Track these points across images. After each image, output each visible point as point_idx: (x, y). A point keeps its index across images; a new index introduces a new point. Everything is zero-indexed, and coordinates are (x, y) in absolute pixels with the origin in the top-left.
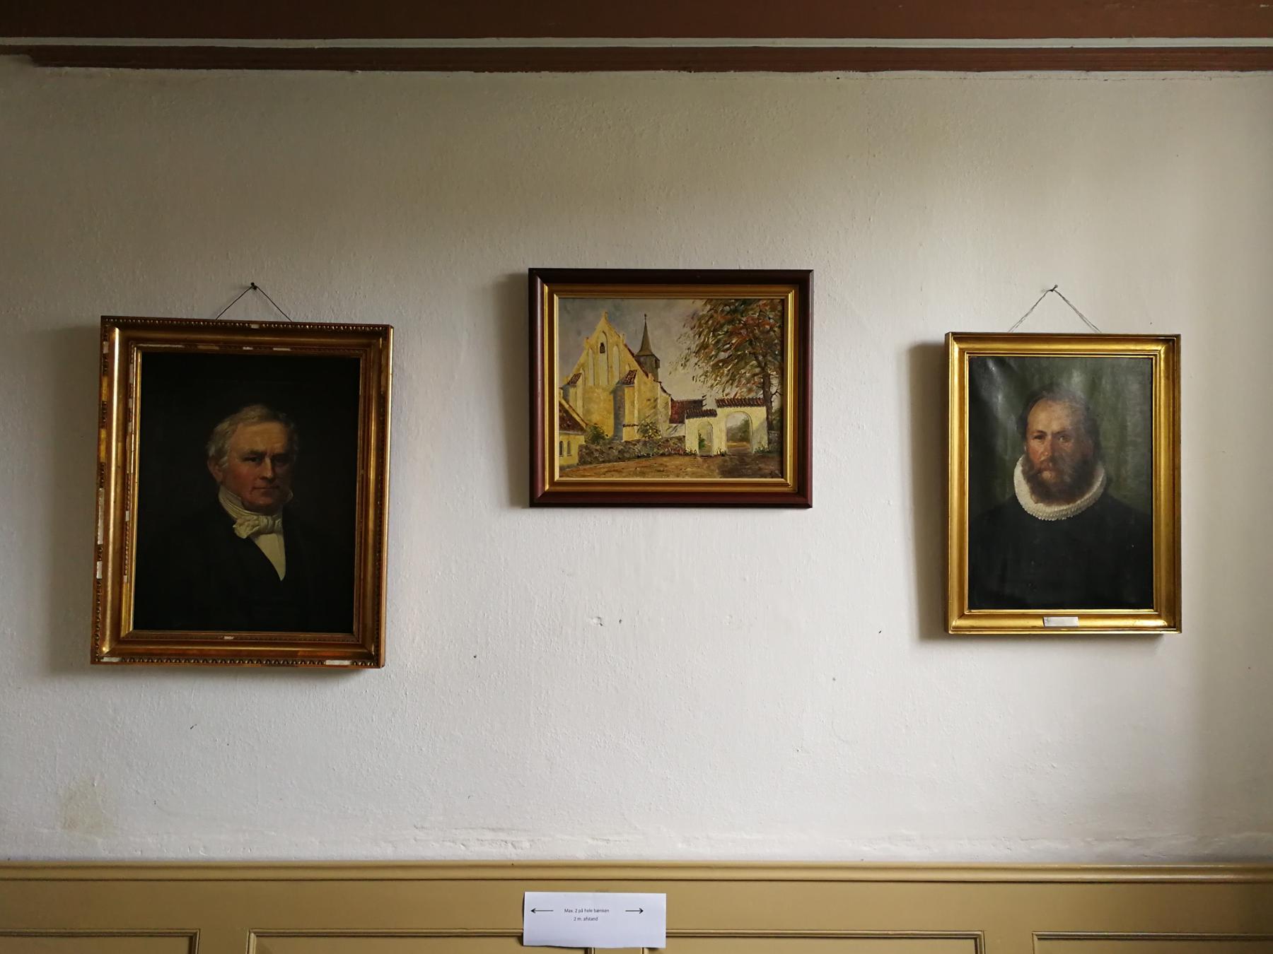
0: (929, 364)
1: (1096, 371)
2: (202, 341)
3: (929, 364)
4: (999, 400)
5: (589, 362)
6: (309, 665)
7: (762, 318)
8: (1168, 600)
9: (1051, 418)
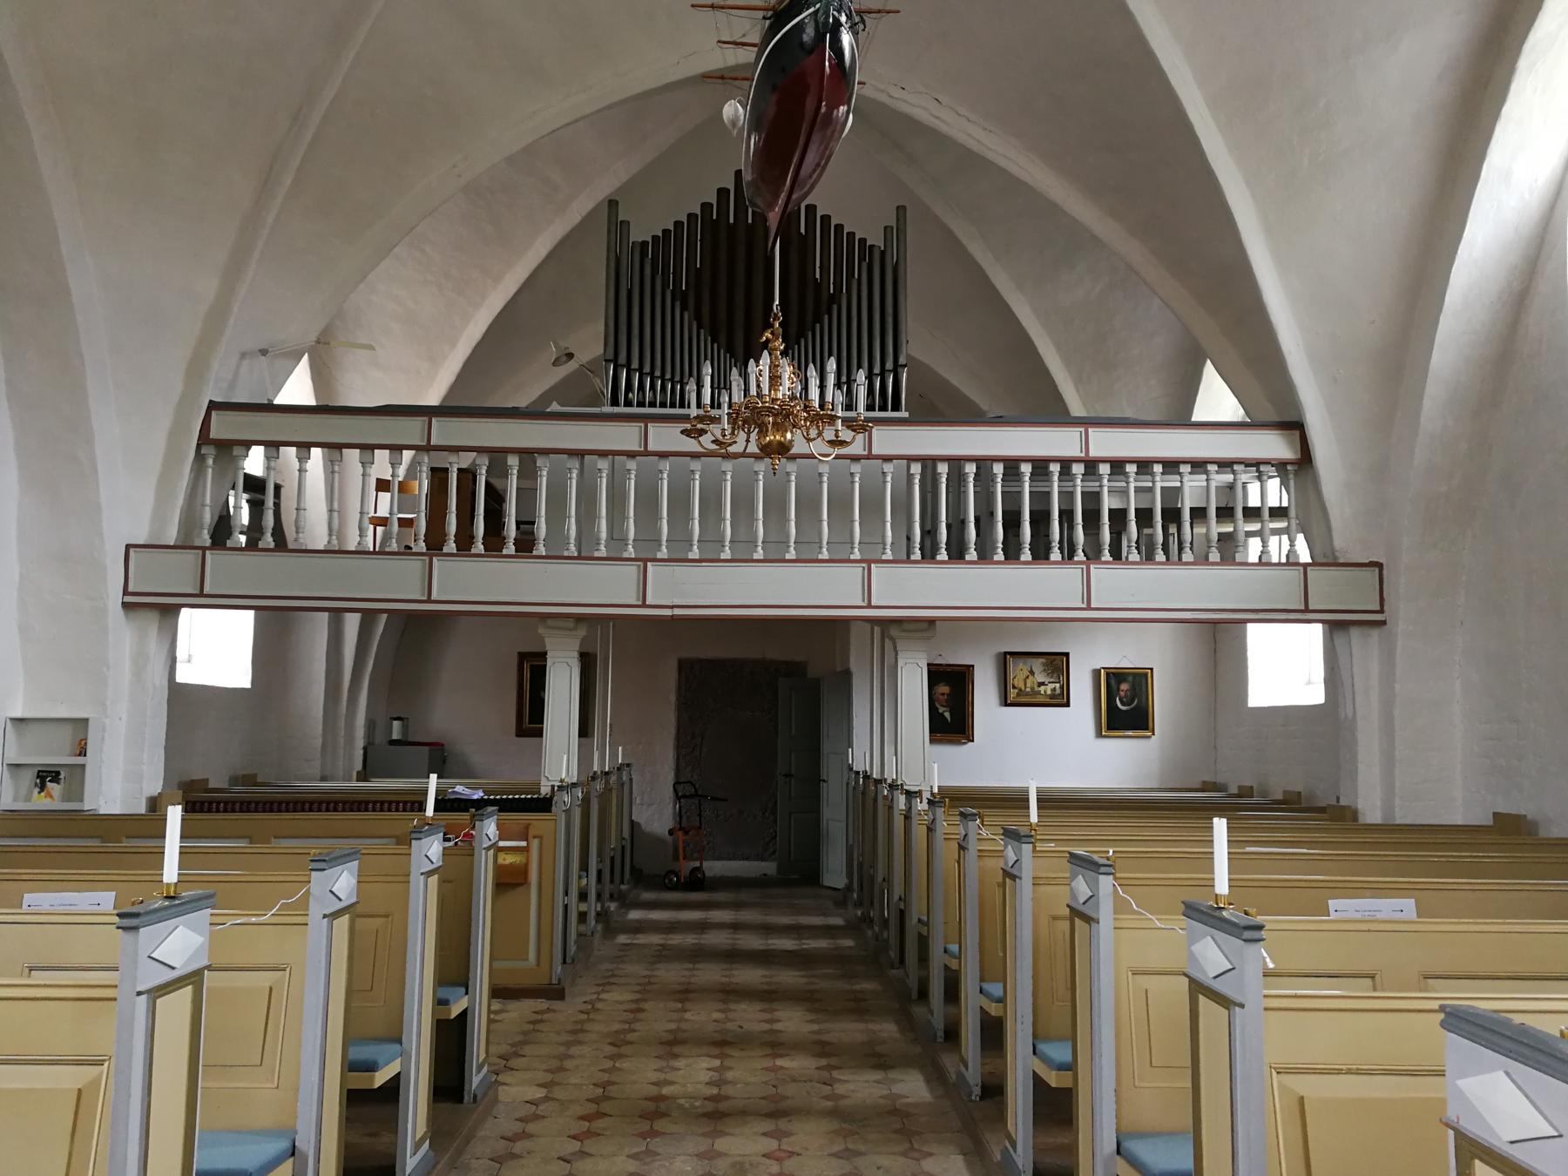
0: (1096, 673)
1: (1135, 675)
2: (700, 386)
3: (1096, 673)
4: (1113, 682)
5: (1018, 672)
6: (959, 743)
7: (1058, 663)
8: (833, 937)
9: (1124, 687)
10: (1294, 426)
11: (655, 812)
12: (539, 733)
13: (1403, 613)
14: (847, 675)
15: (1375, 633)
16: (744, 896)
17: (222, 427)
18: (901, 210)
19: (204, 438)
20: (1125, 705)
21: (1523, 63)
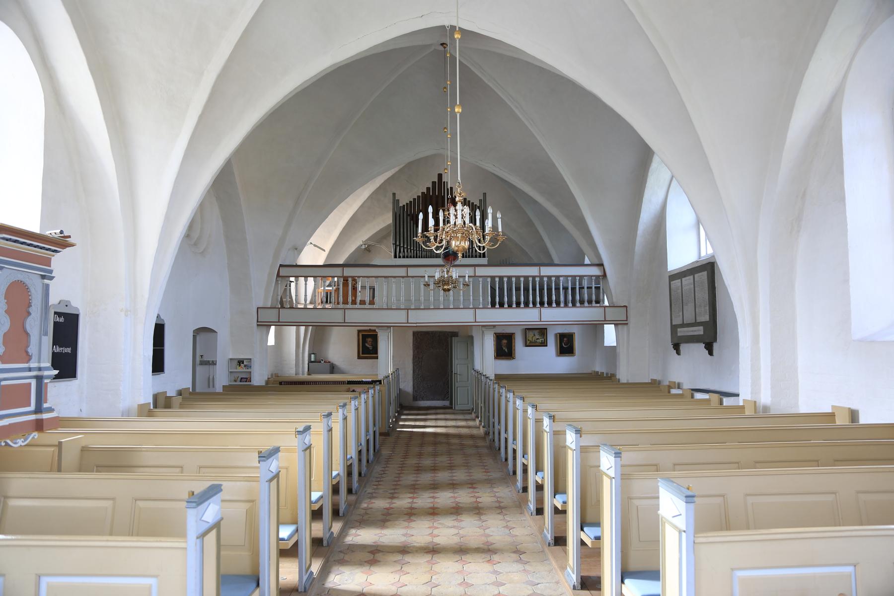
0: (556, 335)
10: (601, 265)
11: (407, 385)
12: (156, 325)
13: (632, 320)
14: (472, 338)
15: (625, 326)
16: (439, 411)
17: (284, 272)
18: (485, 194)
19: (278, 275)
20: (566, 346)
21: (650, 174)
